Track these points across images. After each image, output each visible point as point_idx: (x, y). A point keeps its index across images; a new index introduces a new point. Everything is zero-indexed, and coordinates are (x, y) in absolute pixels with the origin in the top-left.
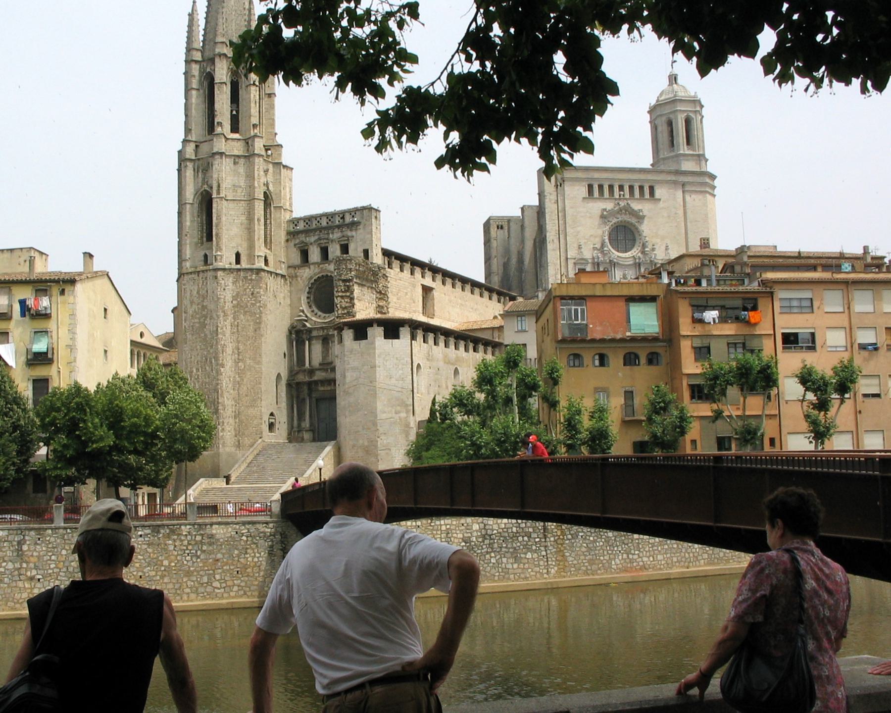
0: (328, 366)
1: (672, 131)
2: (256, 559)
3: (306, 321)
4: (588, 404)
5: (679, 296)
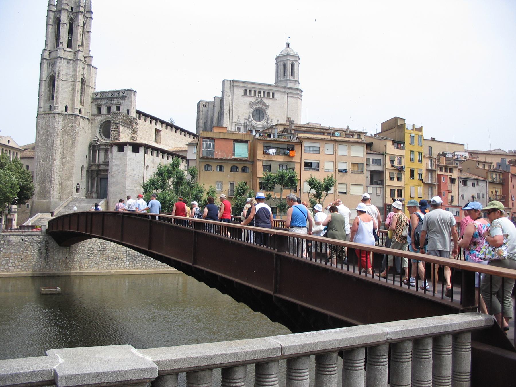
0: (106, 163)
1: (285, 69)
2: (32, 253)
3: (98, 141)
4: (207, 188)
5: (258, 141)
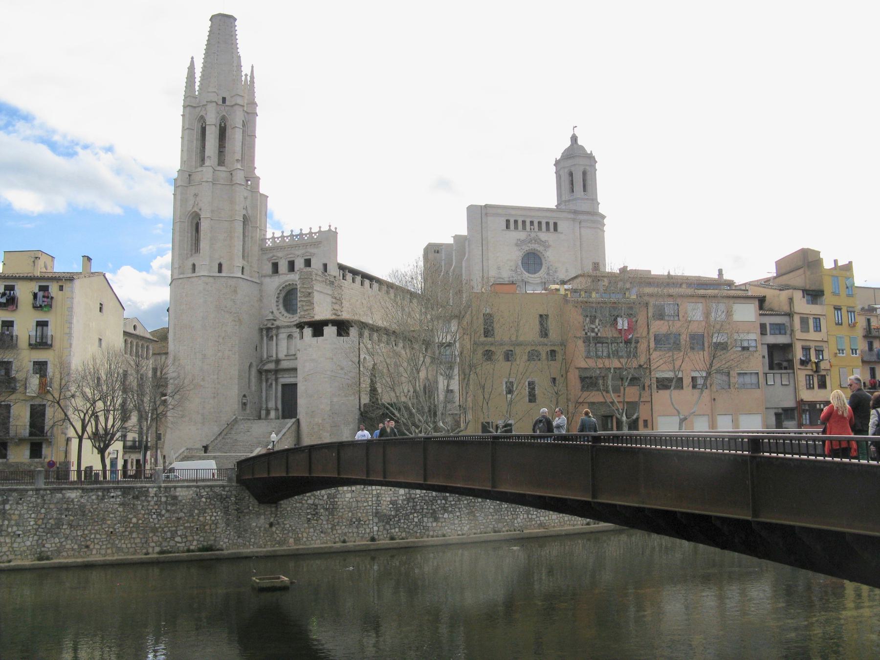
2: (213, 518)
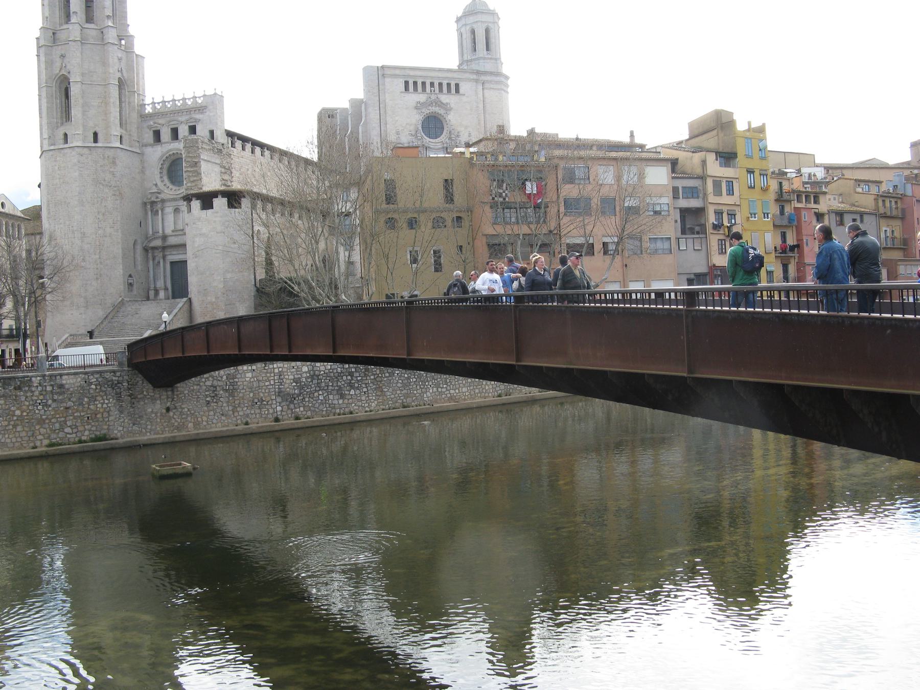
2: (105, 406)
